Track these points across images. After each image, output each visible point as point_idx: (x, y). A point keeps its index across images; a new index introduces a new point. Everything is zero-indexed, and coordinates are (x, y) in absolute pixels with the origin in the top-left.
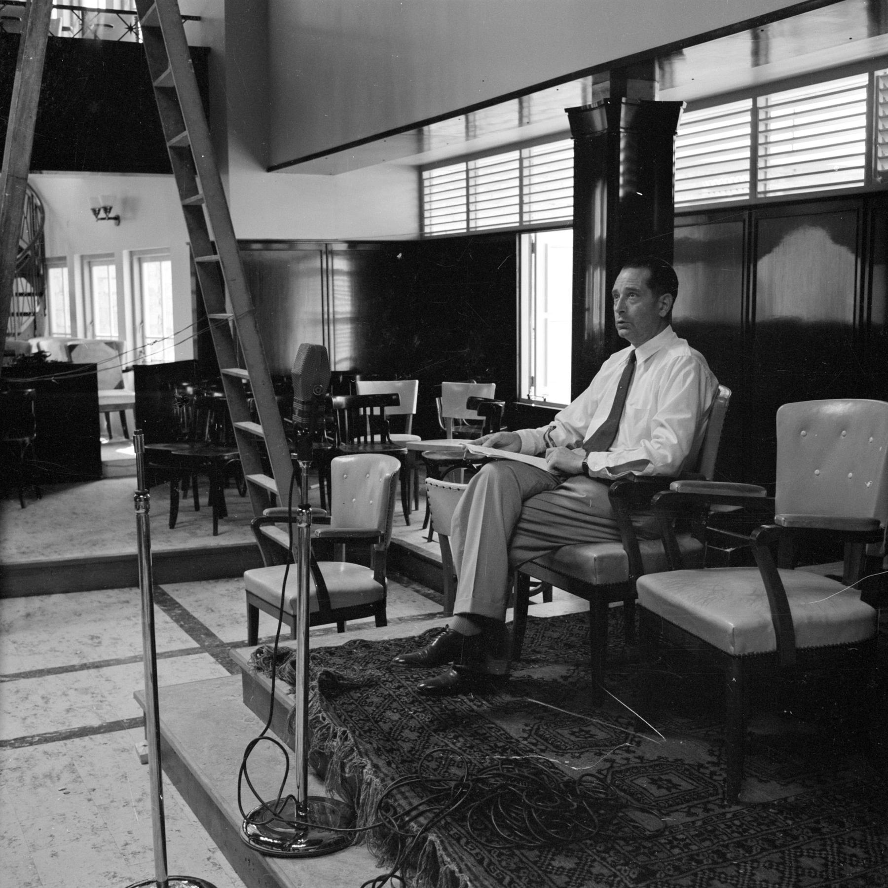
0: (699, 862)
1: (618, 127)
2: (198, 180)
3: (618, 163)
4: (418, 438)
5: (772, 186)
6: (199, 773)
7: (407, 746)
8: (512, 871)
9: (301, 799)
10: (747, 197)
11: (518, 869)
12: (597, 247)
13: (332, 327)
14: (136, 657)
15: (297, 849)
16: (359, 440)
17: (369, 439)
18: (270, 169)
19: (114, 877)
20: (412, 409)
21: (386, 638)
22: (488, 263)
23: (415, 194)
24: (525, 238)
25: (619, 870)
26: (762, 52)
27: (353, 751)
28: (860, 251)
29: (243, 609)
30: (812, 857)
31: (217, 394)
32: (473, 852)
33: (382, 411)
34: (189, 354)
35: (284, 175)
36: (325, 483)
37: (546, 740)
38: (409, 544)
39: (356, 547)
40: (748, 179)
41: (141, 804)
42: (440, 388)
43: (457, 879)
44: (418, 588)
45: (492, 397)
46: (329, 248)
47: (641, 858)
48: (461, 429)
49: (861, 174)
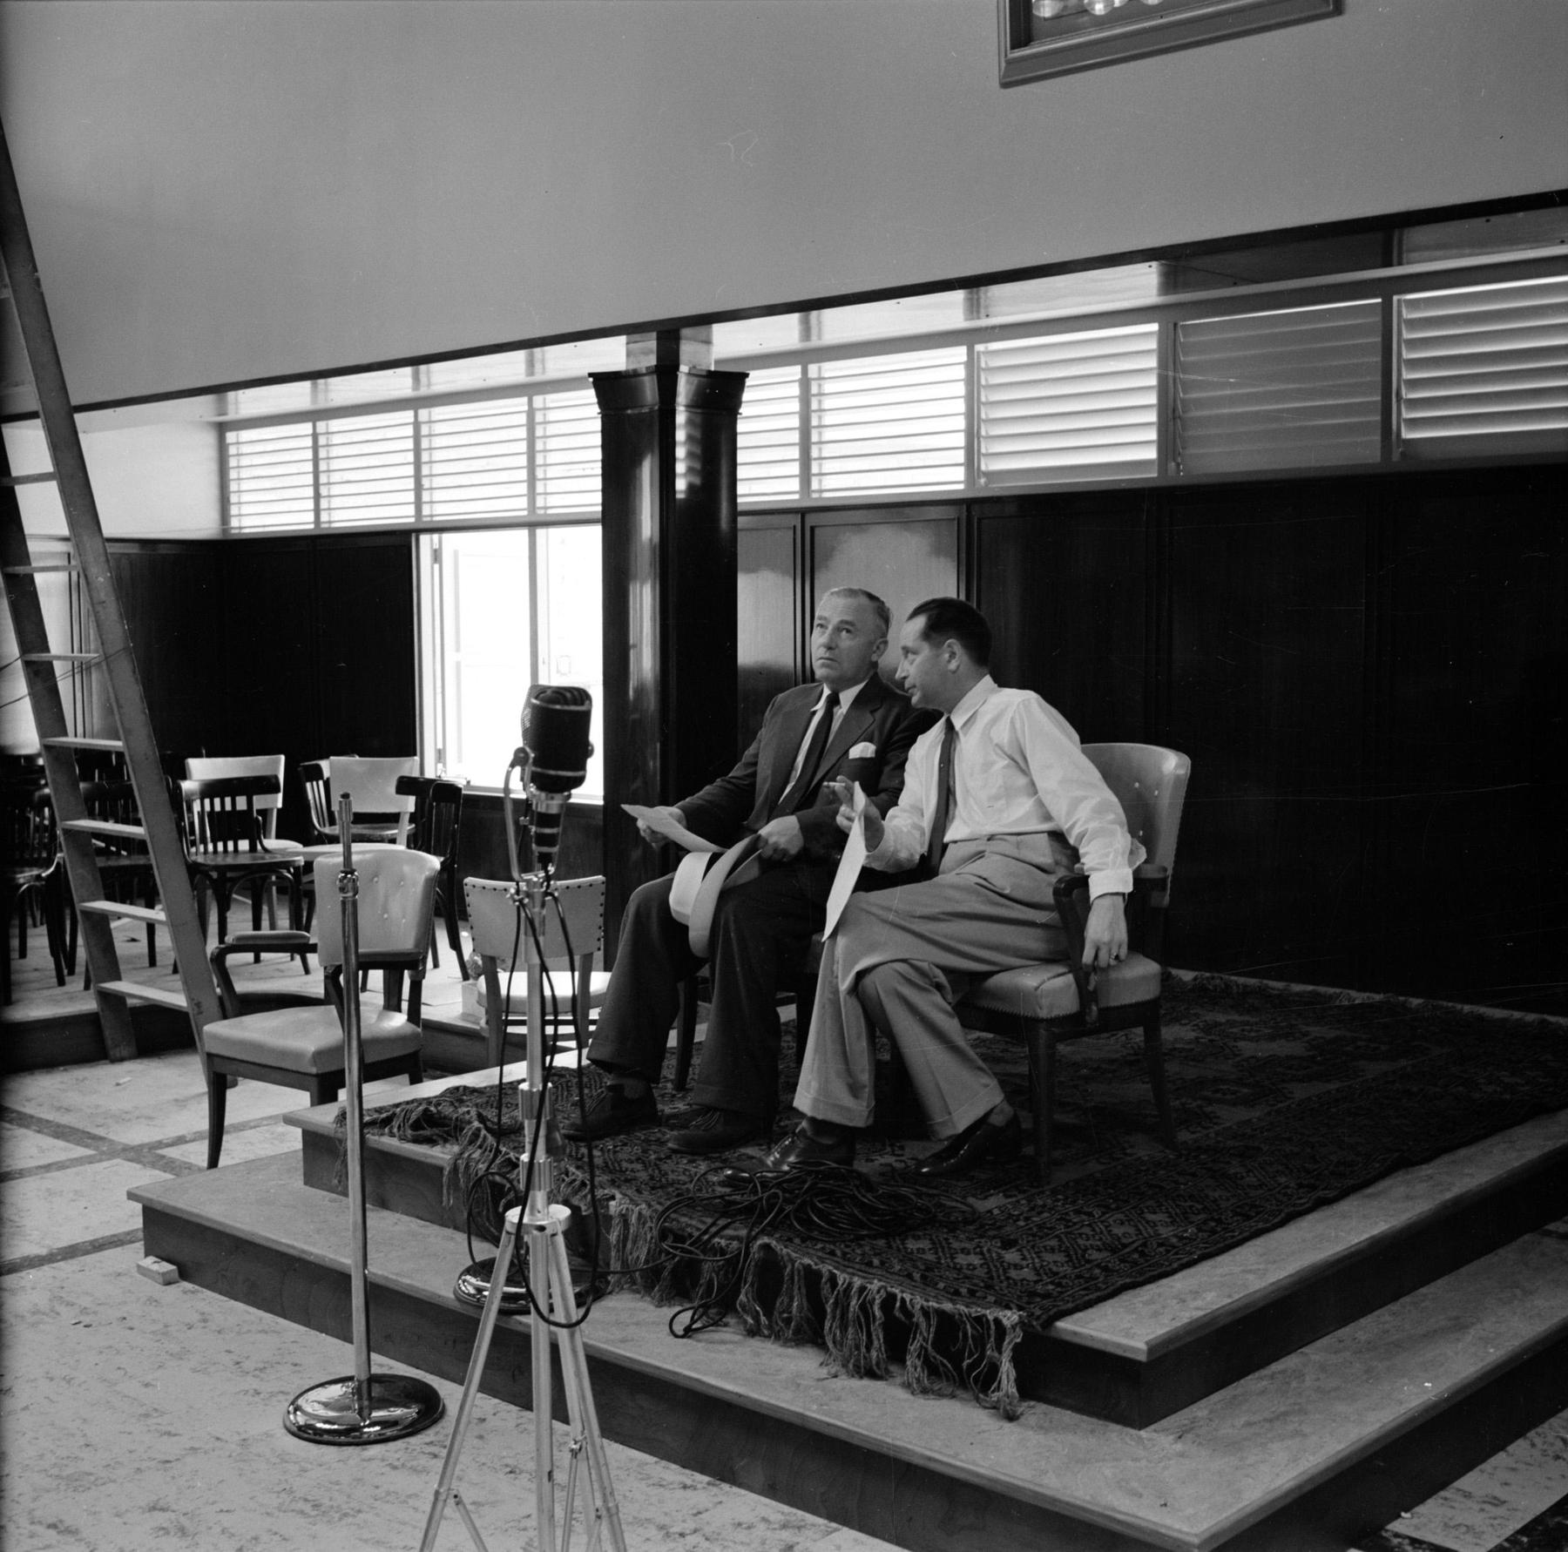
5: (829, 482)
16: (225, 846)
17: (210, 847)
23: (213, 467)
24: (424, 538)
29: (200, 1085)
33: (250, 803)
40: (962, 460)
49: (959, 474)
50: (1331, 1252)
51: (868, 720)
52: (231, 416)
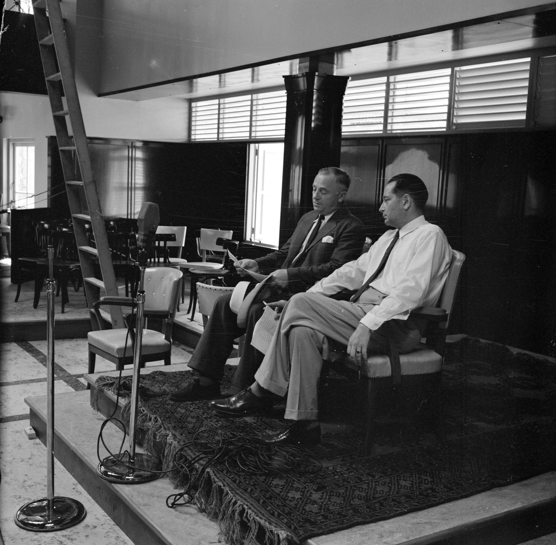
0: (348, 482)
1: (313, 89)
2: (64, 99)
3: (312, 108)
4: (186, 261)
5: (395, 127)
6: (69, 441)
7: (190, 426)
8: (252, 486)
9: (132, 454)
10: (381, 132)
11: (254, 485)
12: (298, 154)
13: (133, 192)
14: (18, 381)
15: (128, 479)
16: (155, 260)
18: (100, 95)
19: (20, 498)
20: (182, 244)
21: (174, 371)
22: (231, 159)
24: (252, 146)
25: (308, 485)
26: (393, 54)
27: (161, 427)
28: (442, 165)
29: (85, 356)
30: (406, 481)
31: (64, 229)
32: (231, 477)
34: (44, 204)
35: (111, 100)
36: (129, 285)
37: (266, 424)
38: (180, 322)
39: (157, 320)
41: (31, 460)
42: (200, 232)
43: (223, 490)
44: (185, 348)
45: (231, 238)
46: (134, 144)
47: (318, 480)
48: (210, 256)
49: (444, 124)
50: (481, 517)
51: (334, 225)
52: (194, 95)
